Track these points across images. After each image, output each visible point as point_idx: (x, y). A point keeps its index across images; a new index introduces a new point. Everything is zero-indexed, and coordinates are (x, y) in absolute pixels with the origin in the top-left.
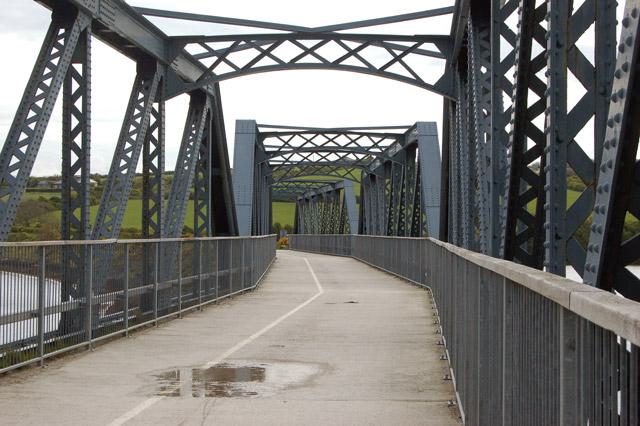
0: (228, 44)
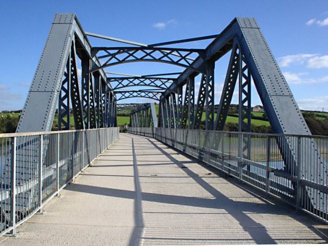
0: (116, 51)
